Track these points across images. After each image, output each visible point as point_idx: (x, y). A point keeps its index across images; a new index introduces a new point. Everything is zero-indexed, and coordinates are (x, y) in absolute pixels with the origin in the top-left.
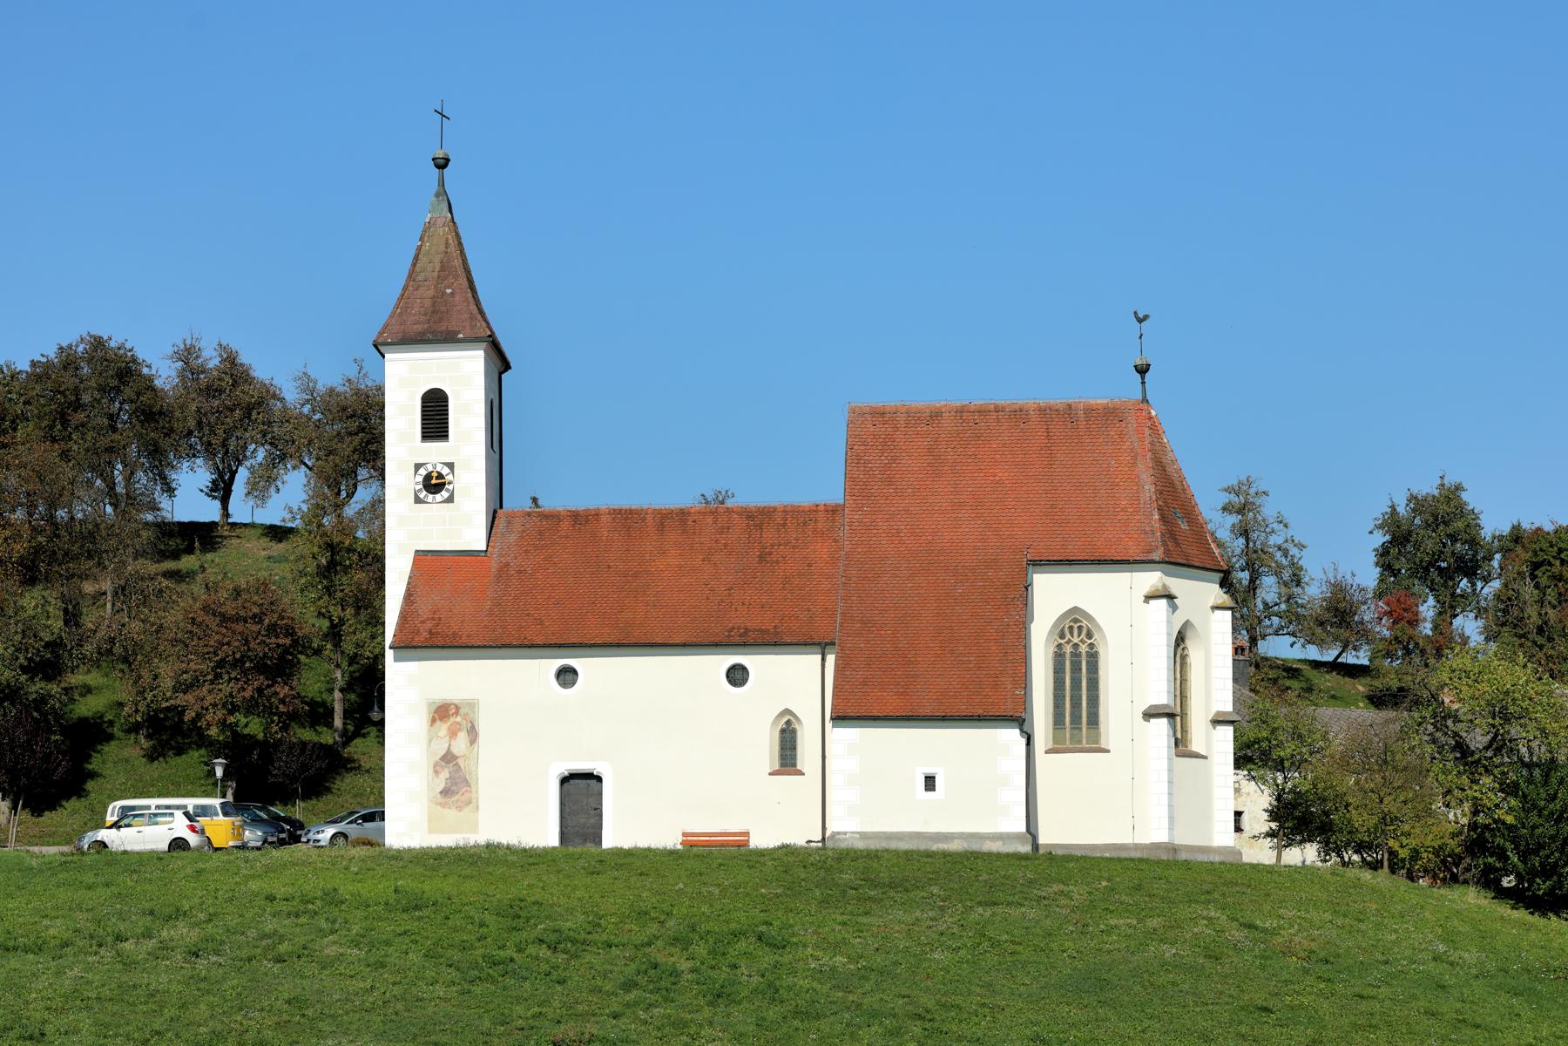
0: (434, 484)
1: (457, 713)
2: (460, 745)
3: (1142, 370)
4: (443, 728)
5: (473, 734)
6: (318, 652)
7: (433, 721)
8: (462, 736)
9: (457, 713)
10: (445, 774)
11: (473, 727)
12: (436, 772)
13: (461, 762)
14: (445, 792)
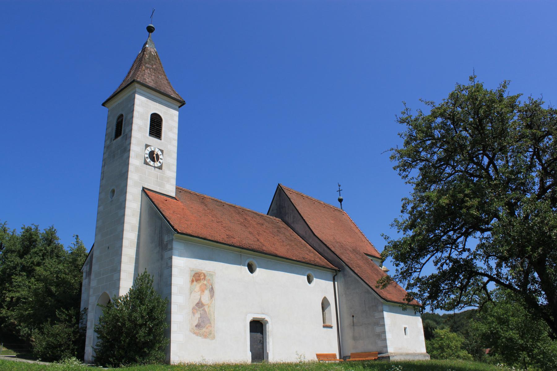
0: (153, 156)
1: (204, 279)
2: (205, 298)
3: (340, 200)
4: (197, 286)
5: (212, 290)
6: (404, 234)
7: (193, 281)
8: (207, 292)
9: (204, 279)
10: (198, 315)
11: (212, 288)
12: (194, 313)
13: (206, 308)
14: (198, 326)
